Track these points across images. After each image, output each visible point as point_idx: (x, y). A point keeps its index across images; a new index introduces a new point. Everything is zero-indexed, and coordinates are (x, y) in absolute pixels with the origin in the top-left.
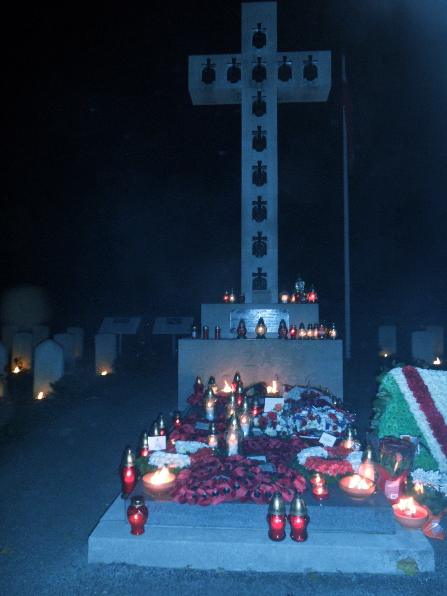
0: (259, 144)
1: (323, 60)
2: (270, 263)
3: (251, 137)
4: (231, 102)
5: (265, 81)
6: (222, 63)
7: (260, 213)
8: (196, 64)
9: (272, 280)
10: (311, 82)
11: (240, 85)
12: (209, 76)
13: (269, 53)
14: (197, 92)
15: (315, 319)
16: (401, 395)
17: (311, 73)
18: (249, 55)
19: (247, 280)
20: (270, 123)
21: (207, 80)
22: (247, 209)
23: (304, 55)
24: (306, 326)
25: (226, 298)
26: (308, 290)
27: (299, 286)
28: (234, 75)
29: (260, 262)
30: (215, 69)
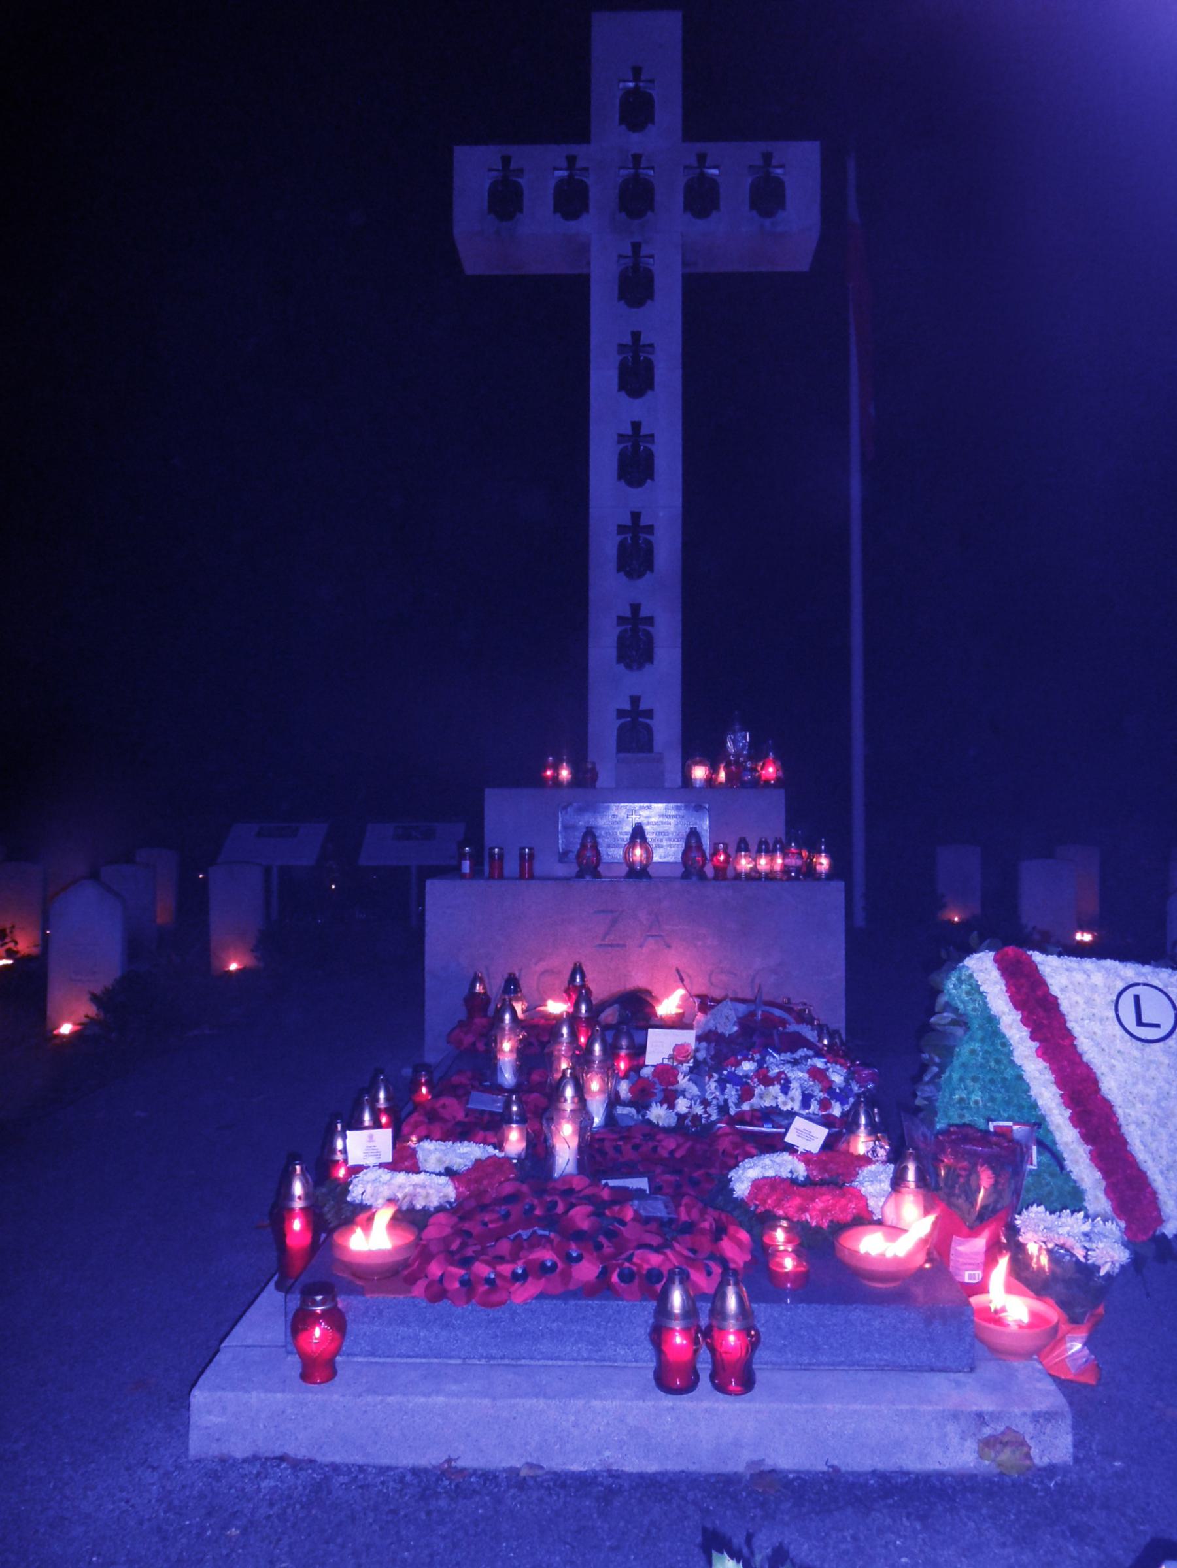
0: (636, 377)
1: (800, 164)
2: (661, 684)
3: (615, 359)
6: (541, 168)
7: (635, 556)
8: (473, 169)
9: (666, 727)
10: (767, 222)
13: (662, 142)
15: (776, 827)
16: (991, 1020)
17: (768, 196)
18: (609, 146)
19: (603, 728)
20: (663, 324)
22: (604, 546)
23: (753, 151)
24: (753, 847)
26: (757, 753)
27: (736, 743)
28: (571, 199)
29: (635, 682)
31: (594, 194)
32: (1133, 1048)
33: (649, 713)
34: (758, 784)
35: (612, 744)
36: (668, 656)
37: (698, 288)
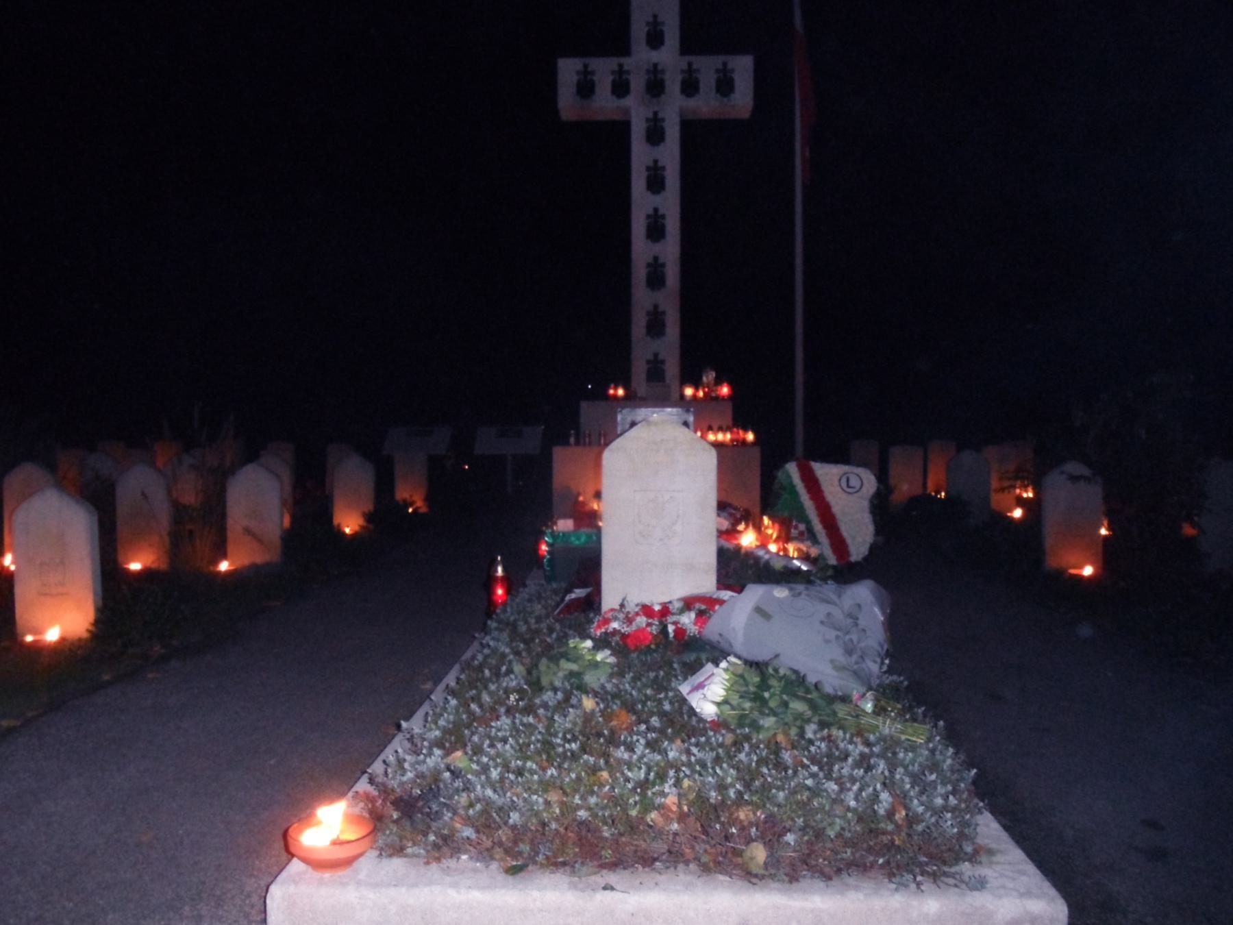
0: (656, 183)
1: (743, 67)
2: (669, 346)
3: (645, 174)
4: (617, 117)
5: (663, 97)
6: (603, 69)
7: (656, 278)
8: (568, 70)
9: (672, 368)
10: (725, 100)
11: (628, 102)
12: (586, 88)
13: (668, 56)
14: (567, 103)
15: (728, 420)
16: (793, 487)
17: (725, 85)
18: (641, 57)
19: (639, 369)
20: (670, 154)
21: (580, 87)
22: (639, 273)
23: (716, 61)
24: (715, 427)
25: (612, 392)
26: (719, 381)
27: (709, 377)
28: (621, 88)
29: (656, 345)
30: (595, 78)
31: (633, 86)
32: (844, 496)
33: (663, 362)
34: (719, 399)
35: (644, 376)
36: (673, 331)
37: (689, 127)
